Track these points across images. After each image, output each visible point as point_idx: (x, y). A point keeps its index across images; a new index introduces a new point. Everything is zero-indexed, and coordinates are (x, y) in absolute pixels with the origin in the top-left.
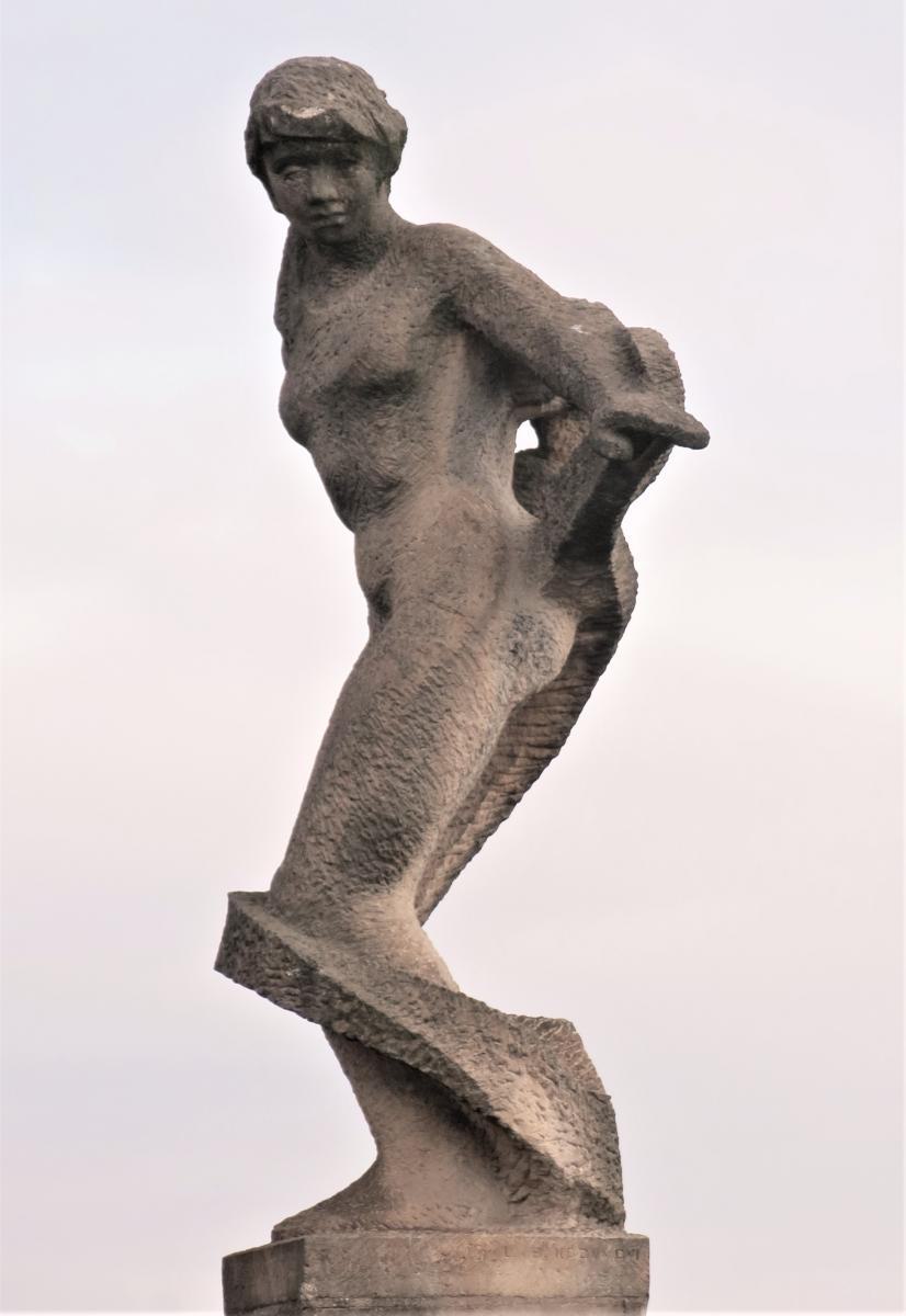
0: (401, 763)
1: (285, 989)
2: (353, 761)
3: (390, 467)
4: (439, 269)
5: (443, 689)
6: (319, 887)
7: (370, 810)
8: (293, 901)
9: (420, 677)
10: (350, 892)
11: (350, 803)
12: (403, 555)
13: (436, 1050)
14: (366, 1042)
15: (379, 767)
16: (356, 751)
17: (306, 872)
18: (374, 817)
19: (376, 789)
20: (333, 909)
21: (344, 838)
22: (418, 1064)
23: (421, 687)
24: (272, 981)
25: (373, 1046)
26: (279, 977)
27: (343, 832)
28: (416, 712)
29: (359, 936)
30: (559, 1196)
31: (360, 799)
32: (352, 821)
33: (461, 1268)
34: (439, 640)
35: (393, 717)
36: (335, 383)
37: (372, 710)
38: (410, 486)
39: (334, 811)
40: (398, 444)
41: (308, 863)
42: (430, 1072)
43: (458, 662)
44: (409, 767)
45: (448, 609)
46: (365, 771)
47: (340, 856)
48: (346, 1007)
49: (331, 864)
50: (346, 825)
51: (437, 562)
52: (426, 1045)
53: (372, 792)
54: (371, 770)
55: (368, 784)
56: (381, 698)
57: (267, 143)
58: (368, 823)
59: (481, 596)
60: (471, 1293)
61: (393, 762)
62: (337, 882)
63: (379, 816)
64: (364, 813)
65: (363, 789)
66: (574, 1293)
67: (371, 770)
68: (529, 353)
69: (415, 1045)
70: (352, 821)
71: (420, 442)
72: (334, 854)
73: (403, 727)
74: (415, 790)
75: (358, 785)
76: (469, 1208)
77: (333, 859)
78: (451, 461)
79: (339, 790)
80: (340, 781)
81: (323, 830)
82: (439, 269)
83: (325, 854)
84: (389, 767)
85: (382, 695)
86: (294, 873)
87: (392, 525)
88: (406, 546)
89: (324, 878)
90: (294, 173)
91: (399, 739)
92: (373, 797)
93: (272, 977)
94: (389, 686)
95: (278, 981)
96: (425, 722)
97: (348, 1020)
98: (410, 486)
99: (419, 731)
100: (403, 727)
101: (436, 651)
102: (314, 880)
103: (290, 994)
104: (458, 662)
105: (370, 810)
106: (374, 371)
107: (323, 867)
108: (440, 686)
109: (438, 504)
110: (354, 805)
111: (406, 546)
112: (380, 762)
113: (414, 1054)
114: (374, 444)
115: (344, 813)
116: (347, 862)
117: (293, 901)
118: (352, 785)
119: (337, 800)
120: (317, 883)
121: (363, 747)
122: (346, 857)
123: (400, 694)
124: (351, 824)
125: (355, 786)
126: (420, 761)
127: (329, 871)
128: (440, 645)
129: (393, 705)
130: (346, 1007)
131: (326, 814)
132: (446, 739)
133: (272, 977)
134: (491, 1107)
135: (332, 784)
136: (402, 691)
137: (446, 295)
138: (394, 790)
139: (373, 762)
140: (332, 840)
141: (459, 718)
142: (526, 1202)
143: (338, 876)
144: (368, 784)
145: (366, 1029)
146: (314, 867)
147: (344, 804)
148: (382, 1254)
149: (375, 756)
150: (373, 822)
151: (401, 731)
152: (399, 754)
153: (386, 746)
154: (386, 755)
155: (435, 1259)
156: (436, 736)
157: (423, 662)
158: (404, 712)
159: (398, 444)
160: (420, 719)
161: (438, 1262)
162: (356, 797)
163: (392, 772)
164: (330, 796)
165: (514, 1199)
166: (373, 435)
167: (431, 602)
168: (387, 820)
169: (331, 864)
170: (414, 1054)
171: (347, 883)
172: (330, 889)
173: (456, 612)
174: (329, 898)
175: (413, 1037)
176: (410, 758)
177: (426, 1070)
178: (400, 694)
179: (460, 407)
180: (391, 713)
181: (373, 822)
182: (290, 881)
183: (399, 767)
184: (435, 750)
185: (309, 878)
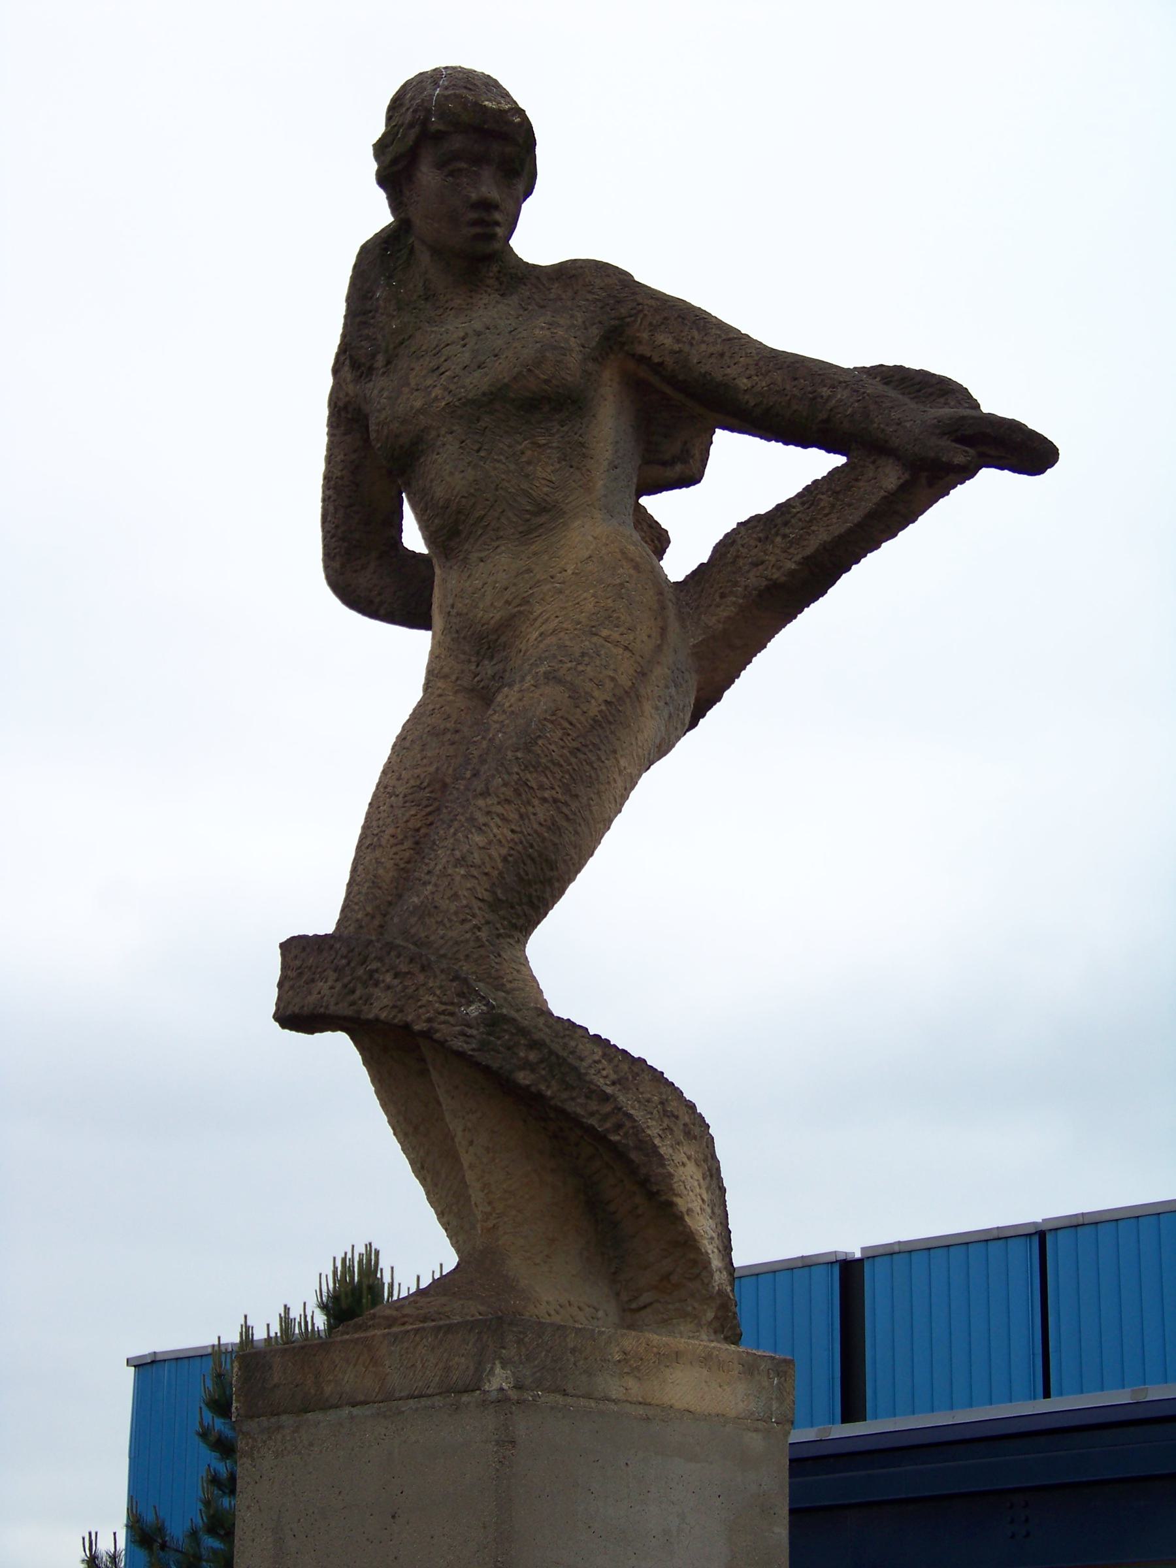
0: (567, 798)
1: (458, 1028)
2: (515, 790)
3: (546, 489)
4: (609, 295)
5: (613, 727)
6: (467, 926)
7: (532, 846)
8: (432, 938)
9: (593, 709)
10: (499, 936)
11: (510, 835)
12: (546, 588)
13: (630, 1116)
14: (552, 1098)
15: (544, 800)
16: (520, 779)
17: (453, 908)
18: (535, 855)
19: (541, 824)
20: (482, 952)
21: (501, 874)
22: (607, 1130)
23: (593, 720)
24: (442, 1018)
25: (559, 1104)
26: (452, 1014)
27: (500, 865)
28: (586, 746)
29: (509, 986)
30: (696, 1305)
31: (522, 832)
32: (511, 855)
33: (639, 1371)
34: (611, 673)
35: (563, 747)
36: (484, 394)
37: (539, 737)
38: (565, 513)
39: (490, 842)
40: (558, 466)
41: (455, 896)
42: (620, 1142)
43: (628, 700)
44: (574, 805)
45: (617, 644)
46: (529, 803)
47: (494, 893)
48: (533, 1056)
49: (482, 900)
50: (505, 859)
51: (593, 596)
52: (620, 1109)
53: (536, 826)
54: (536, 802)
55: (532, 817)
56: (550, 726)
57: (439, 131)
58: (529, 862)
59: (649, 636)
60: (648, 1400)
61: (559, 796)
62: (488, 923)
63: (540, 855)
64: (525, 848)
65: (526, 821)
66: (733, 1414)
67: (536, 802)
68: (743, 383)
69: (607, 1108)
70: (511, 855)
71: (578, 468)
72: (486, 890)
73: (573, 760)
74: (576, 833)
75: (521, 816)
76: (597, 1310)
77: (487, 896)
78: (605, 496)
79: (497, 819)
80: (499, 809)
81: (477, 861)
82: (609, 295)
83: (478, 889)
84: (555, 801)
85: (552, 722)
86: (436, 907)
87: (535, 554)
88: (552, 577)
89: (474, 916)
90: (460, 170)
91: (568, 772)
92: (536, 831)
93: (443, 1013)
94: (560, 713)
95: (451, 1020)
96: (594, 759)
97: (533, 1071)
98: (565, 513)
99: (587, 768)
100: (573, 760)
101: (609, 685)
102: (462, 917)
103: (465, 1035)
104: (628, 700)
105: (532, 846)
106: (546, 382)
107: (476, 904)
108: (610, 723)
109: (590, 538)
110: (515, 836)
111: (552, 577)
112: (547, 794)
113: (606, 1117)
114: (529, 463)
115: (503, 846)
116: (500, 900)
117: (432, 938)
118: (513, 816)
119: (495, 830)
120: (463, 921)
121: (529, 776)
122: (500, 896)
123: (571, 724)
124: (510, 859)
125: (517, 817)
126: (584, 801)
127: (480, 908)
128: (613, 679)
129: (564, 734)
130: (533, 1056)
131: (481, 845)
132: (609, 783)
133: (443, 1013)
134: (672, 1189)
135: (488, 813)
136: (574, 721)
137: (617, 322)
138: (559, 828)
139: (539, 793)
140: (486, 874)
141: (623, 762)
142: (648, 1310)
143: (491, 917)
144: (532, 817)
145: (553, 1083)
146: (465, 902)
147: (506, 837)
148: (571, 1345)
149: (541, 787)
150: (533, 860)
151: (571, 764)
152: (567, 790)
153: (554, 778)
154: (553, 788)
155: (617, 1357)
156: (602, 777)
157: (596, 693)
158: (575, 744)
159: (558, 466)
160: (589, 755)
161: (619, 1361)
162: (518, 829)
163: (558, 808)
164: (484, 825)
165: (634, 1306)
166: (529, 453)
167: (596, 634)
168: (547, 860)
169: (482, 900)
170: (606, 1117)
171: (499, 926)
172: (479, 929)
173: (626, 648)
174: (478, 939)
175: (606, 1098)
176: (577, 796)
177: (615, 1138)
178: (571, 724)
179: (617, 442)
180: (561, 743)
181: (533, 860)
182: (430, 915)
183: (566, 804)
184: (598, 793)
185: (456, 913)
